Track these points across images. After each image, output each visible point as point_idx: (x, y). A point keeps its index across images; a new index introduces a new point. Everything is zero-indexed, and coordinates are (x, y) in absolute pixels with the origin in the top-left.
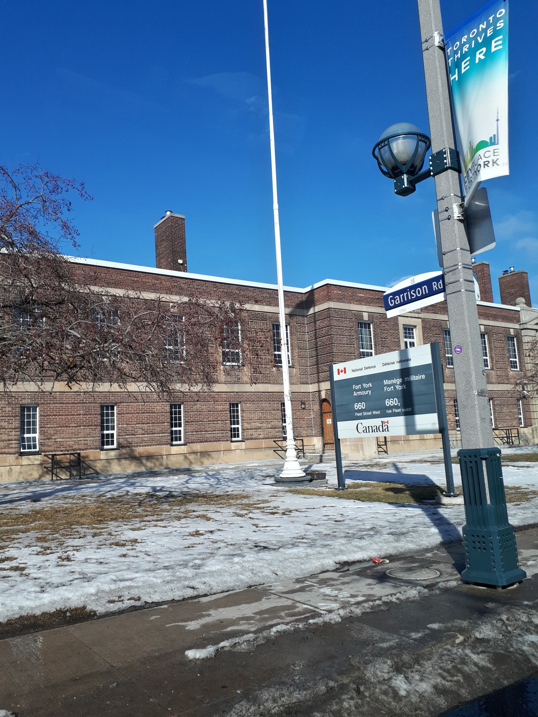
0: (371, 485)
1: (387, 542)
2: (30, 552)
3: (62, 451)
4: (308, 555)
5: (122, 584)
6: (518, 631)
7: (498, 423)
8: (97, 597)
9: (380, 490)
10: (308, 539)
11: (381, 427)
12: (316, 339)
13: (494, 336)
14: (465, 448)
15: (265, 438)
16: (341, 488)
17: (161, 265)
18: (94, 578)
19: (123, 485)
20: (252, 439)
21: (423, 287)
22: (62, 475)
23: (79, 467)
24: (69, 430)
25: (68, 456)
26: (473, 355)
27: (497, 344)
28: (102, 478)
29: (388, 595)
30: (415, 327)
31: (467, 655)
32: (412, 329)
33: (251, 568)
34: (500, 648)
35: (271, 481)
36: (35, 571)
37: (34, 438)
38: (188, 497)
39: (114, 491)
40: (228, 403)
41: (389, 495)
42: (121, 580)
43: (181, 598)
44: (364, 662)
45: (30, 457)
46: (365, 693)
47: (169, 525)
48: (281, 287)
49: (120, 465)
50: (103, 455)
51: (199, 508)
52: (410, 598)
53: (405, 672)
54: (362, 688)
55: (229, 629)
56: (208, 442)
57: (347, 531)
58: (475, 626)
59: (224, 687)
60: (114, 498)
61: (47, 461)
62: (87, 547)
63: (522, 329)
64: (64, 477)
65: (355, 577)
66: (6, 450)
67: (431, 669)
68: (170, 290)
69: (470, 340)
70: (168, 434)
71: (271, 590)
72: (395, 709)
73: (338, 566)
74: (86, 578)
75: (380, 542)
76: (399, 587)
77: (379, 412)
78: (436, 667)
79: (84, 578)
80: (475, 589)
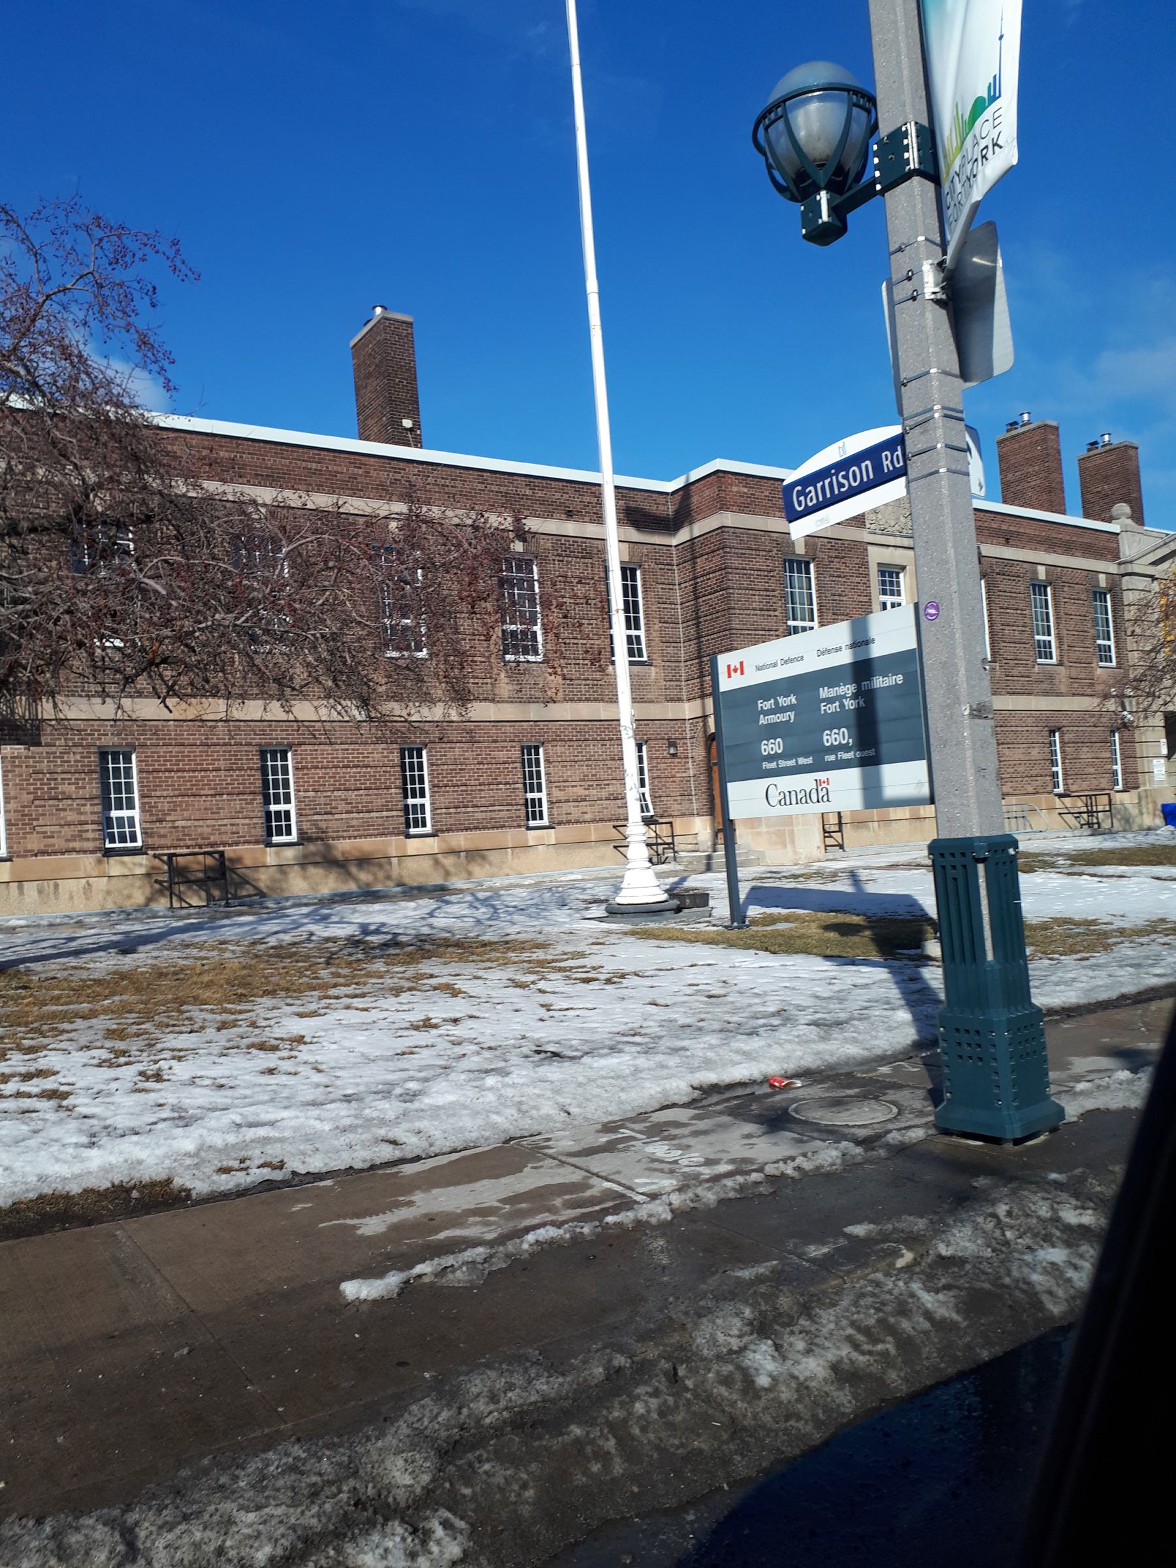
0: (797, 918)
1: (803, 1041)
2: (85, 1060)
3: (188, 847)
4: (637, 1071)
5: (251, 1134)
6: (1027, 1240)
7: (1070, 782)
8: (196, 1161)
9: (814, 930)
10: (646, 1034)
11: (814, 791)
13: (1066, 589)
14: (944, 835)
16: (735, 924)
17: (367, 433)
18: (200, 1118)
19: (305, 921)
20: (569, 822)
21: (863, 465)
22: (191, 898)
23: (223, 882)
24: (200, 802)
25: (201, 857)
26: (961, 623)
27: (1072, 608)
28: (271, 904)
29: (777, 1162)
30: (903, 568)
31: (912, 1295)
32: (898, 574)
33: (517, 1099)
34: (983, 1278)
35: (598, 911)
36: (87, 1101)
37: (131, 820)
38: (427, 947)
39: (284, 932)
40: (518, 745)
41: (828, 940)
42: (251, 1125)
43: (366, 1165)
44: (695, 1313)
45: (126, 859)
46: (687, 1382)
47: (373, 1005)
48: (608, 479)
49: (305, 878)
50: (271, 857)
51: (439, 969)
52: (822, 1167)
53: (776, 1333)
54: (681, 1372)
55: (442, 1235)
57: (727, 1017)
58: (939, 1229)
59: (402, 1364)
60: (281, 947)
61: (159, 869)
62: (201, 1051)
63: (1124, 575)
64: (195, 902)
65: (725, 1119)
66: (77, 845)
67: (832, 1326)
69: (955, 588)
70: (399, 813)
71: (548, 1147)
72: (745, 1416)
73: (697, 1094)
74: (183, 1119)
75: (789, 1041)
76: (805, 1142)
77: (810, 760)
78: (844, 1322)
79: (180, 1118)
80: (959, 1146)
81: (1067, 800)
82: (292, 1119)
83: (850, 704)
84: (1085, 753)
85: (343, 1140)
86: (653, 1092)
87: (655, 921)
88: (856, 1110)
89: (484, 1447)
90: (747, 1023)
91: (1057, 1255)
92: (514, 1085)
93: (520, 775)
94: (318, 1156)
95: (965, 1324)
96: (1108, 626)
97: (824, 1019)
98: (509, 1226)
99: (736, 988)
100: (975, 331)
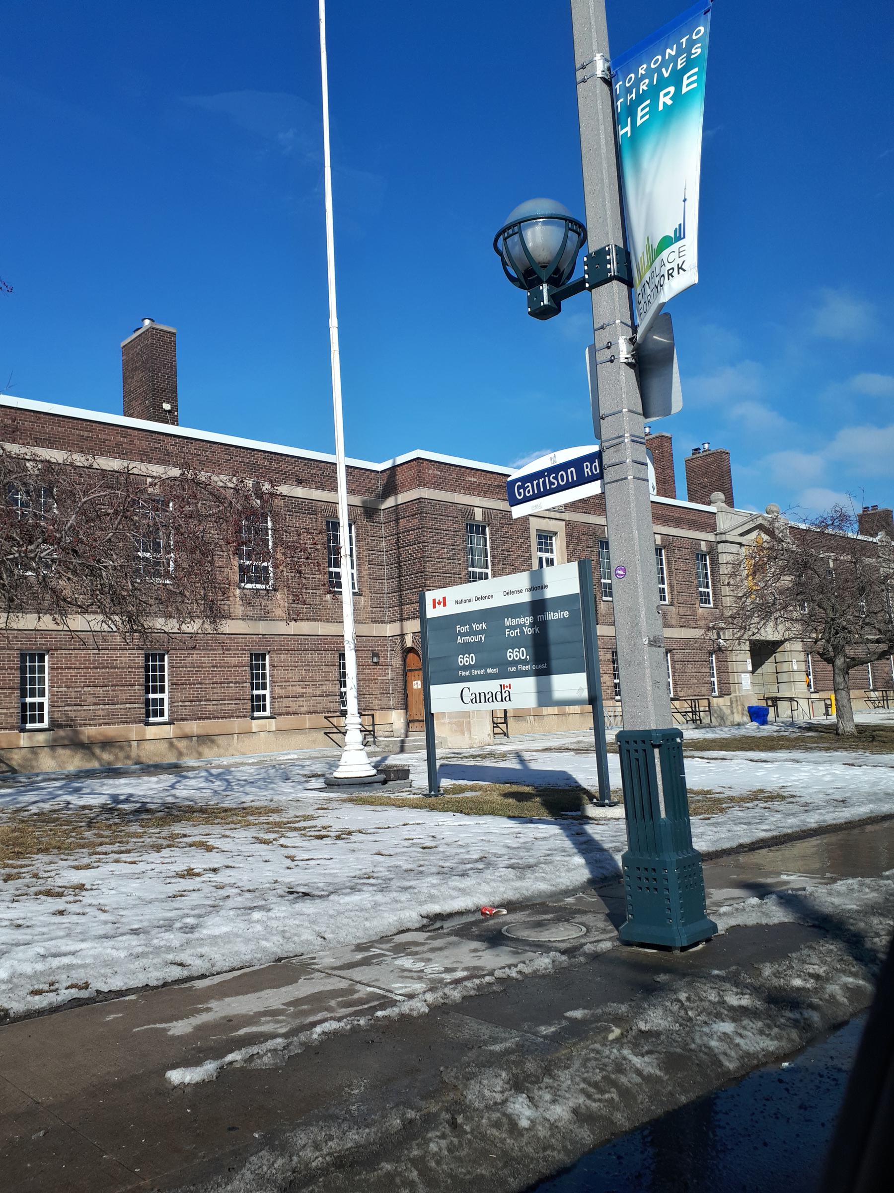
0: (481, 788)
1: (504, 880)
4: (376, 905)
5: (56, 962)
6: (703, 1018)
7: (679, 689)
8: (10, 986)
9: (495, 797)
11: (499, 693)
12: (399, 548)
13: (676, 551)
14: (628, 728)
15: (311, 713)
17: (132, 411)
19: (60, 792)
20: (287, 714)
21: (569, 471)
26: (643, 581)
27: (680, 565)
28: (23, 779)
29: (504, 968)
30: (555, 534)
31: (625, 1058)
34: (675, 1045)
39: (43, 801)
40: (248, 653)
42: (55, 956)
43: (160, 983)
44: (464, 1077)
47: (140, 859)
48: (341, 460)
49: (53, 758)
50: (24, 740)
51: (194, 831)
52: (538, 970)
54: (460, 1119)
55: (242, 1032)
56: (211, 718)
57: (441, 863)
58: (639, 1011)
60: (43, 813)
63: (719, 543)
65: (453, 939)
67: (569, 1082)
68: (147, 456)
69: (638, 557)
70: (141, 706)
72: (512, 1149)
73: (425, 921)
77: (496, 671)
78: (577, 1079)
80: (639, 953)
81: (677, 703)
82: (89, 949)
83: (528, 631)
84: (690, 668)
85: (138, 964)
86: (391, 921)
87: (366, 791)
88: (554, 930)
89: (315, 1183)
90: (457, 867)
91: (727, 1027)
92: (276, 918)
93: (249, 676)
94: (117, 977)
95: (667, 1078)
96: (707, 578)
97: (518, 863)
98: (297, 1022)
99: (443, 841)
100: (655, 385)
